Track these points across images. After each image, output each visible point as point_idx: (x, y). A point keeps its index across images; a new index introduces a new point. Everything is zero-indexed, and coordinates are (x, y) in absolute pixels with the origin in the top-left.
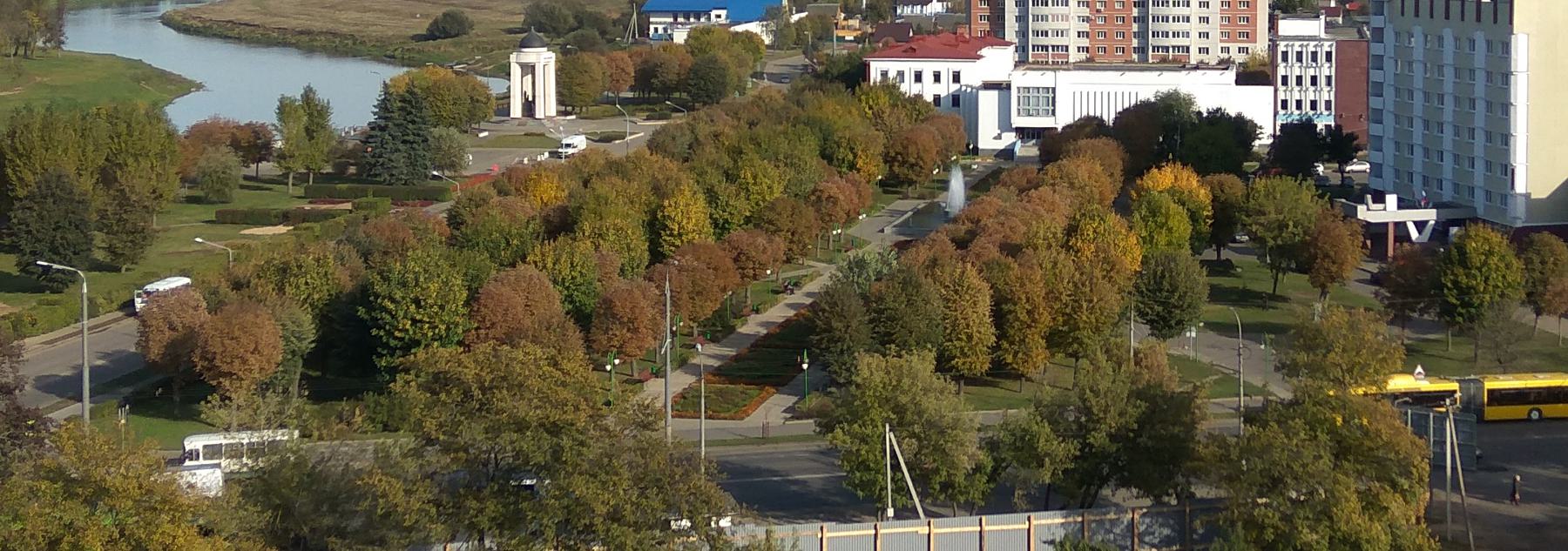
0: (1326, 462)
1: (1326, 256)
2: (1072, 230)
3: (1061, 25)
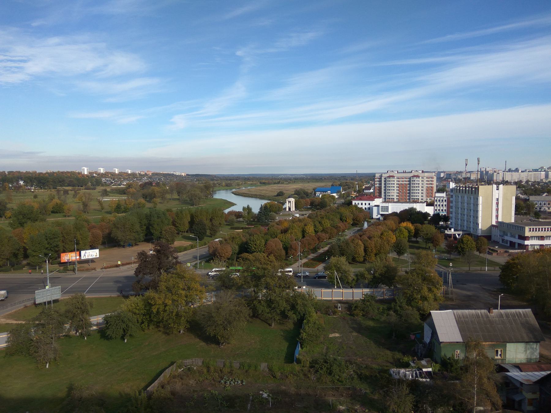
0: (420, 281)
1: (436, 240)
2: (382, 234)
3: (393, 194)
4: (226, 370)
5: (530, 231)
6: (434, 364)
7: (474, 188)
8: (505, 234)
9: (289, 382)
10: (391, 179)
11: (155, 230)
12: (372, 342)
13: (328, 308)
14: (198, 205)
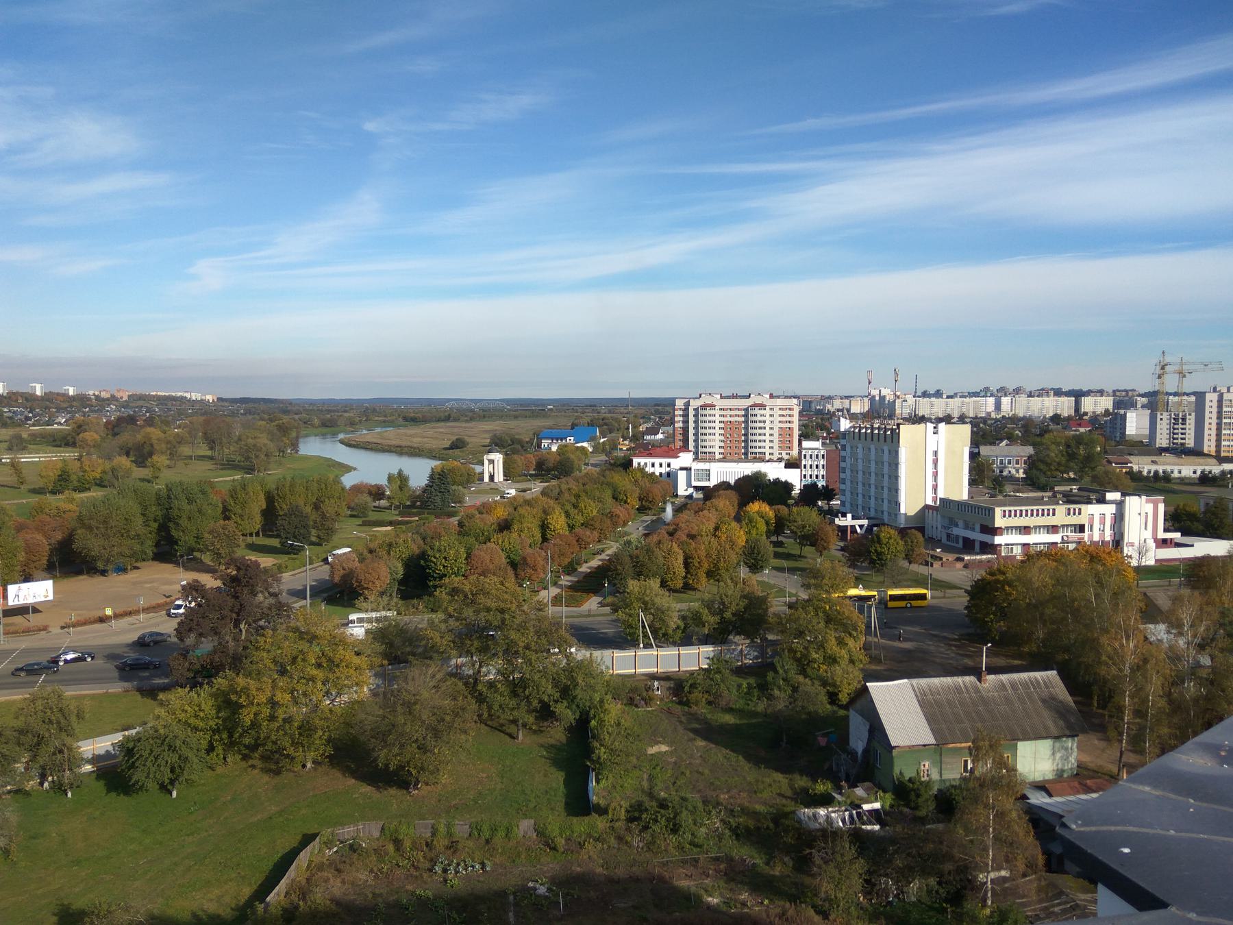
0: (822, 624)
3: (712, 444)
4: (441, 842)
5: (1004, 516)
6: (880, 793)
7: (889, 429)
8: (952, 522)
9: (585, 857)
10: (708, 411)
11: (183, 531)
12: (741, 758)
13: (634, 690)
14: (265, 470)
